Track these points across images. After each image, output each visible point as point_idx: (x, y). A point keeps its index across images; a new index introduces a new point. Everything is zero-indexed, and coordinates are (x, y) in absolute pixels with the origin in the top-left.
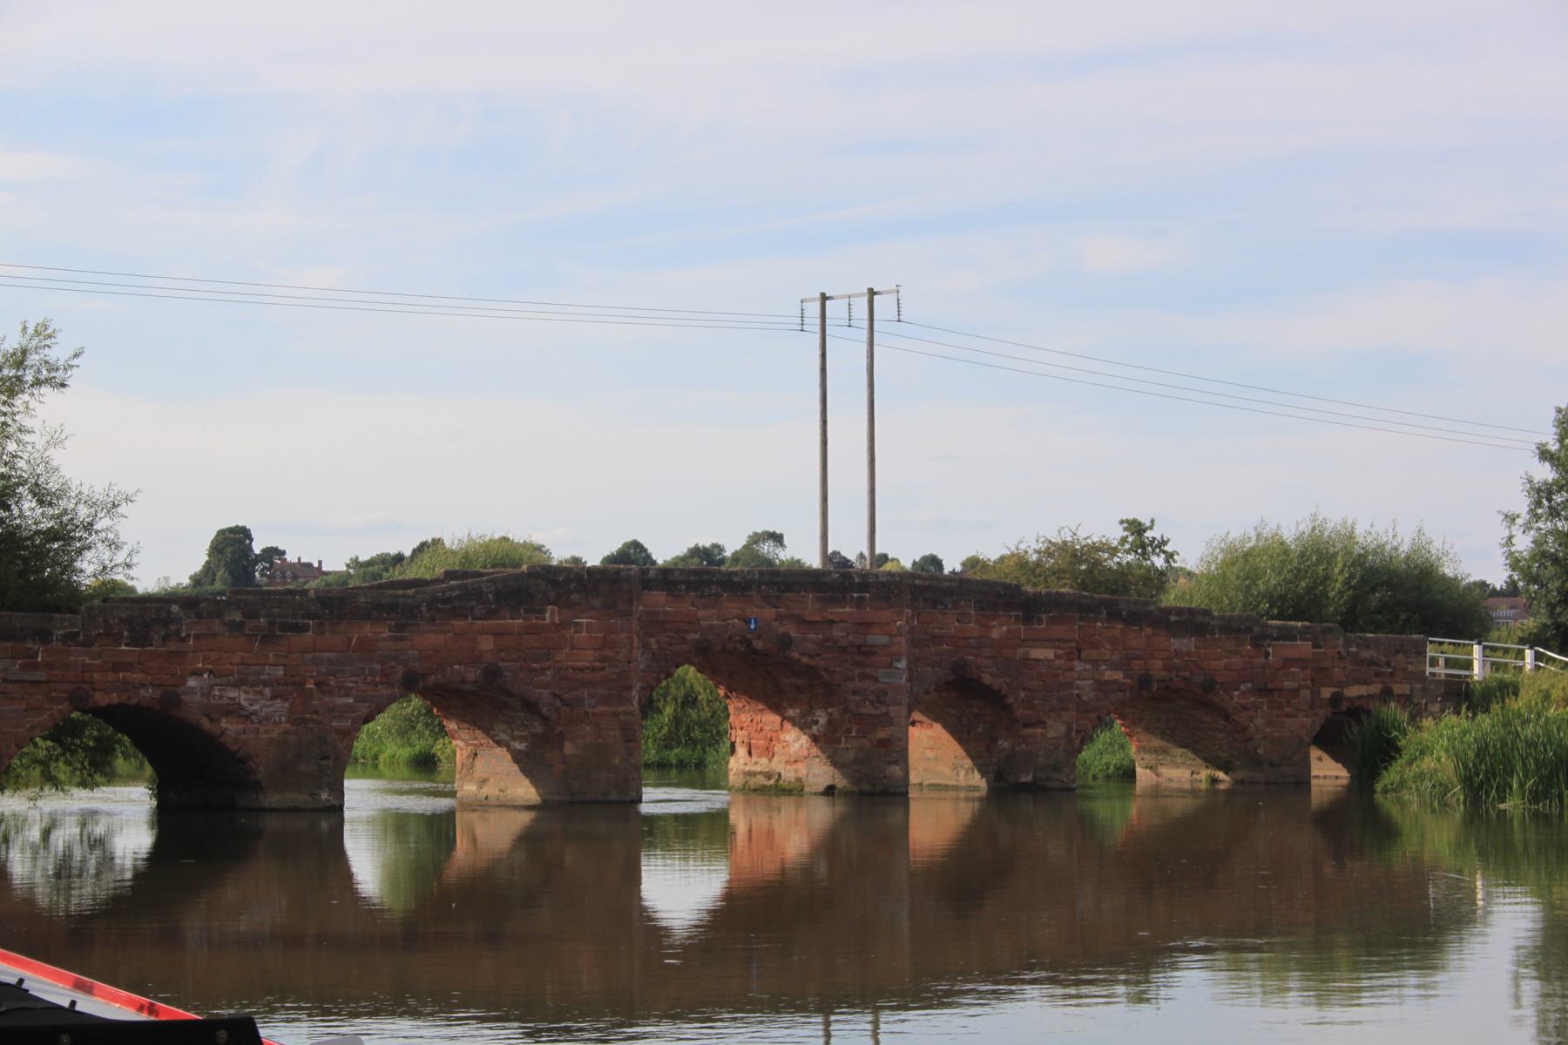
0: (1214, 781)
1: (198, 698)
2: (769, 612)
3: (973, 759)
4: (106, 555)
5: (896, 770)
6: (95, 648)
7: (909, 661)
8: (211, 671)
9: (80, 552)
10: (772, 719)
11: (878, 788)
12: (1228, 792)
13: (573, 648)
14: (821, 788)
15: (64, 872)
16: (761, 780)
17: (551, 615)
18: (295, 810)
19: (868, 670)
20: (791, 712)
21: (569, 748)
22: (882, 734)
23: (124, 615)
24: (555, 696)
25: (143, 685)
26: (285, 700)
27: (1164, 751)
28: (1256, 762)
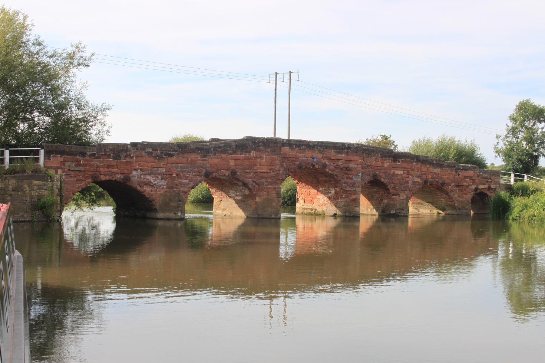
0: (439, 213)
1: (136, 178)
2: (320, 156)
3: (373, 205)
4: (100, 128)
5: (357, 208)
6: (101, 160)
7: (362, 174)
8: (141, 169)
9: (92, 126)
10: (313, 191)
11: (352, 215)
12: (443, 217)
13: (260, 165)
14: (332, 214)
15: (83, 237)
16: (309, 211)
17: (253, 154)
18: (169, 219)
19: (349, 176)
20: (321, 189)
21: (258, 199)
22: (353, 197)
23: (111, 148)
24: (254, 181)
25: (118, 173)
26: (166, 180)
27: (422, 204)
28: (454, 208)
